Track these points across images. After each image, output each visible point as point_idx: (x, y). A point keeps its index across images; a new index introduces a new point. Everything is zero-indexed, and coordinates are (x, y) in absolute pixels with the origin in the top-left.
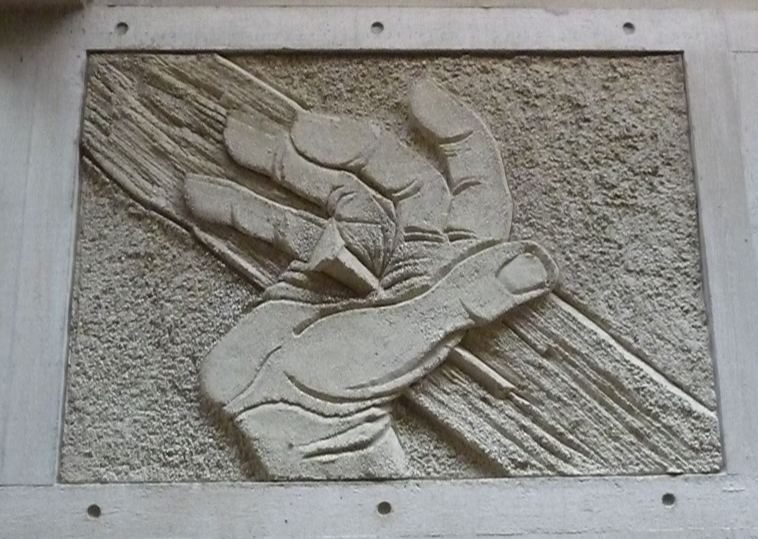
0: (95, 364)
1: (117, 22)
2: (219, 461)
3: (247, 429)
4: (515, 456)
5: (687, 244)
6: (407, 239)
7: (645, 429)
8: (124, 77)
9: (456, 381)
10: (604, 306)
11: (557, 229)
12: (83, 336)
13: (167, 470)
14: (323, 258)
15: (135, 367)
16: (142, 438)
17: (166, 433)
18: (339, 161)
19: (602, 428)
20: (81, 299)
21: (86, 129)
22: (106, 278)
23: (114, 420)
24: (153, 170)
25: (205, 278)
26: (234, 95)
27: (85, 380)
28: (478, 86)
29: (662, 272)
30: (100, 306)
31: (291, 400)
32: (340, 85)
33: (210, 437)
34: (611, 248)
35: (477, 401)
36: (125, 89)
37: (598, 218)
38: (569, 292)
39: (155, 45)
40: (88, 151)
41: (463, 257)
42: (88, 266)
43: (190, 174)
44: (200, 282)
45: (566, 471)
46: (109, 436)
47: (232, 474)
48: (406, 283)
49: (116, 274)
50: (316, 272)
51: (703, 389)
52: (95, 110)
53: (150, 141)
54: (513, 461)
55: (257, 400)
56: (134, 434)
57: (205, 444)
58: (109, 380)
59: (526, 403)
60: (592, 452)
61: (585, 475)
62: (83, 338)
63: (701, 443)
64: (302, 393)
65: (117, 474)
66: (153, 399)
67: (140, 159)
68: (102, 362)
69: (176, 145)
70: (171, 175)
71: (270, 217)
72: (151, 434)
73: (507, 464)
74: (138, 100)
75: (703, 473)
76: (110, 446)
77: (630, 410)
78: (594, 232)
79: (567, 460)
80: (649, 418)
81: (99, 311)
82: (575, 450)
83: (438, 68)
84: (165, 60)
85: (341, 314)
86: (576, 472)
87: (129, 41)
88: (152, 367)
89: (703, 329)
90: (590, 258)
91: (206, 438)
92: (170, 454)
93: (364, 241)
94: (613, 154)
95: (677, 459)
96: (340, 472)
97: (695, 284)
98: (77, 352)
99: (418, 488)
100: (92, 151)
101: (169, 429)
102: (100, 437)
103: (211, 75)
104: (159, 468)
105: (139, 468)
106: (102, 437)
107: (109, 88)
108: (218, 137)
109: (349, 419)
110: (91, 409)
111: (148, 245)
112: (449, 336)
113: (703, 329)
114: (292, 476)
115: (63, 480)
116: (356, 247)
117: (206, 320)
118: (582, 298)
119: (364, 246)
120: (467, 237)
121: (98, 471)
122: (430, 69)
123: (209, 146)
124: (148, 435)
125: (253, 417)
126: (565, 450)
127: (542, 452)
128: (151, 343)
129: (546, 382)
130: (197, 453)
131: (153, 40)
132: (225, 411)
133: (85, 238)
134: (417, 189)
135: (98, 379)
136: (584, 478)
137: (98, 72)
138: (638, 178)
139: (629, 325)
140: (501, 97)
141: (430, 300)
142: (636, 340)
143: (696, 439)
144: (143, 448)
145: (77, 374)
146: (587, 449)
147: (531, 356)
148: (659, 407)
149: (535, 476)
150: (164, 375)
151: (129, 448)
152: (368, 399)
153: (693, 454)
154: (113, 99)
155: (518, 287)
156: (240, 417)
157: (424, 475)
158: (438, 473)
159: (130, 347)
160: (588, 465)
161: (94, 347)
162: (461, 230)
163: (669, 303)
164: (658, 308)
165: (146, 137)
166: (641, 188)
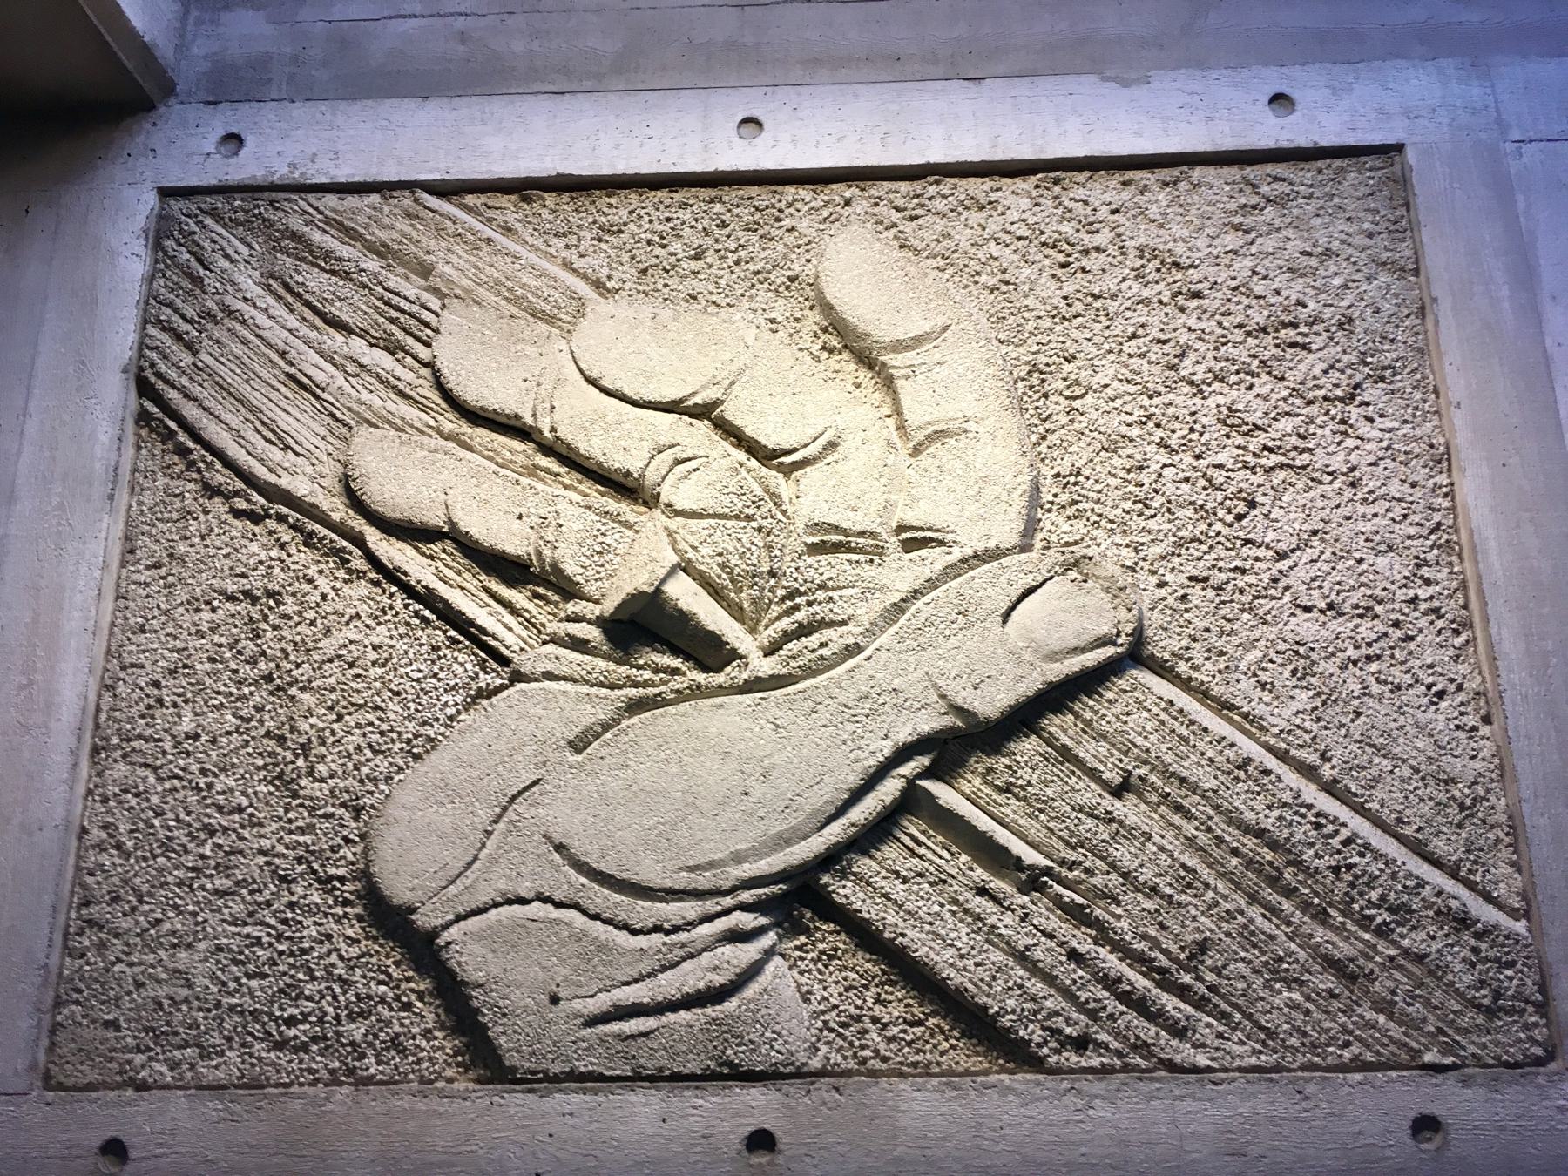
0: (141, 825)
1: (221, 132)
2: (397, 1035)
3: (459, 963)
4: (1059, 1022)
5: (1432, 547)
6: (814, 549)
7: (1361, 961)
8: (233, 239)
9: (922, 851)
10: (1247, 684)
11: (1136, 522)
12: (121, 766)
13: (284, 1057)
14: (629, 589)
15: (225, 830)
16: (232, 985)
17: (285, 974)
18: (668, 394)
19: (1259, 959)
20: (121, 688)
21: (148, 342)
22: (179, 644)
23: (174, 946)
24: (285, 422)
25: (388, 641)
26: (457, 268)
27: (118, 861)
28: (963, 237)
29: (1378, 609)
30: (160, 701)
31: (558, 896)
32: (676, 246)
33: (381, 983)
34: (1257, 559)
35: (969, 895)
36: (232, 261)
37: (1226, 498)
38: (1167, 656)
39: (296, 175)
40: (153, 385)
41: (933, 584)
42: (140, 620)
43: (364, 429)
44: (375, 648)
45: (1178, 1058)
46: (159, 982)
47: (426, 1065)
48: (813, 640)
49: (201, 635)
50: (619, 621)
51: (1492, 870)
52: (170, 305)
53: (282, 363)
54: (1055, 1032)
55: (483, 899)
56: (213, 978)
57: (370, 997)
58: (169, 858)
59: (1079, 900)
60: (1238, 1016)
61: (1226, 1070)
62: (122, 769)
63: (1497, 995)
64: (583, 880)
65: (172, 1069)
66: (261, 899)
67: (257, 399)
68: (156, 822)
69: (337, 373)
70: (323, 431)
71: (523, 510)
72: (249, 976)
73: (1039, 1040)
74: (259, 284)
75: (1507, 1065)
76: (160, 1004)
77: (1321, 917)
78: (1218, 526)
79: (1179, 1032)
80: (1367, 936)
81: (158, 713)
82: (1198, 1007)
83: (876, 205)
84: (316, 204)
85: (671, 709)
86: (1202, 1060)
87: (245, 168)
88: (263, 831)
89: (1481, 733)
90: (1211, 582)
91: (372, 984)
92: (291, 1022)
93: (720, 554)
94: (1256, 362)
95: (1441, 1031)
96: (661, 1060)
97: (1457, 632)
98: (105, 800)
99: (837, 1096)
100: (160, 385)
101: (292, 966)
102: (139, 985)
103: (408, 230)
104: (264, 1054)
105: (222, 1054)
106: (142, 985)
107: (200, 261)
108: (424, 353)
109: (683, 936)
110: (125, 924)
111: (268, 575)
112: (903, 754)
113: (1481, 733)
114: (555, 1069)
115: (53, 1082)
116: (702, 567)
117: (385, 727)
118: (1196, 668)
119: (719, 565)
120: (941, 543)
121: (129, 1062)
122: (860, 207)
123: (406, 375)
124: (244, 980)
125: (479, 937)
126: (1170, 1003)
127: (1122, 1013)
128: (265, 778)
129: (1124, 854)
130: (352, 1018)
131: (292, 166)
132: (414, 922)
133: (138, 561)
134: (832, 446)
135: (145, 859)
136: (1223, 1075)
137: (181, 231)
138: (1314, 410)
139: (1307, 725)
140: (1007, 256)
141: (862, 675)
142: (1324, 758)
143: (1482, 983)
144: (232, 1008)
145: (100, 847)
146: (1224, 1006)
147: (1089, 794)
148: (1391, 910)
149: (1105, 1071)
150: (287, 847)
151: (200, 1009)
152: (726, 893)
153: (1480, 1020)
154: (207, 281)
155: (1056, 646)
156: (445, 936)
157: (852, 1065)
158: (885, 1060)
159: (218, 787)
160: (1230, 1046)
161: (141, 789)
162: (930, 529)
163: (1397, 675)
164: (1375, 688)
165: (275, 357)
166: (1319, 432)
